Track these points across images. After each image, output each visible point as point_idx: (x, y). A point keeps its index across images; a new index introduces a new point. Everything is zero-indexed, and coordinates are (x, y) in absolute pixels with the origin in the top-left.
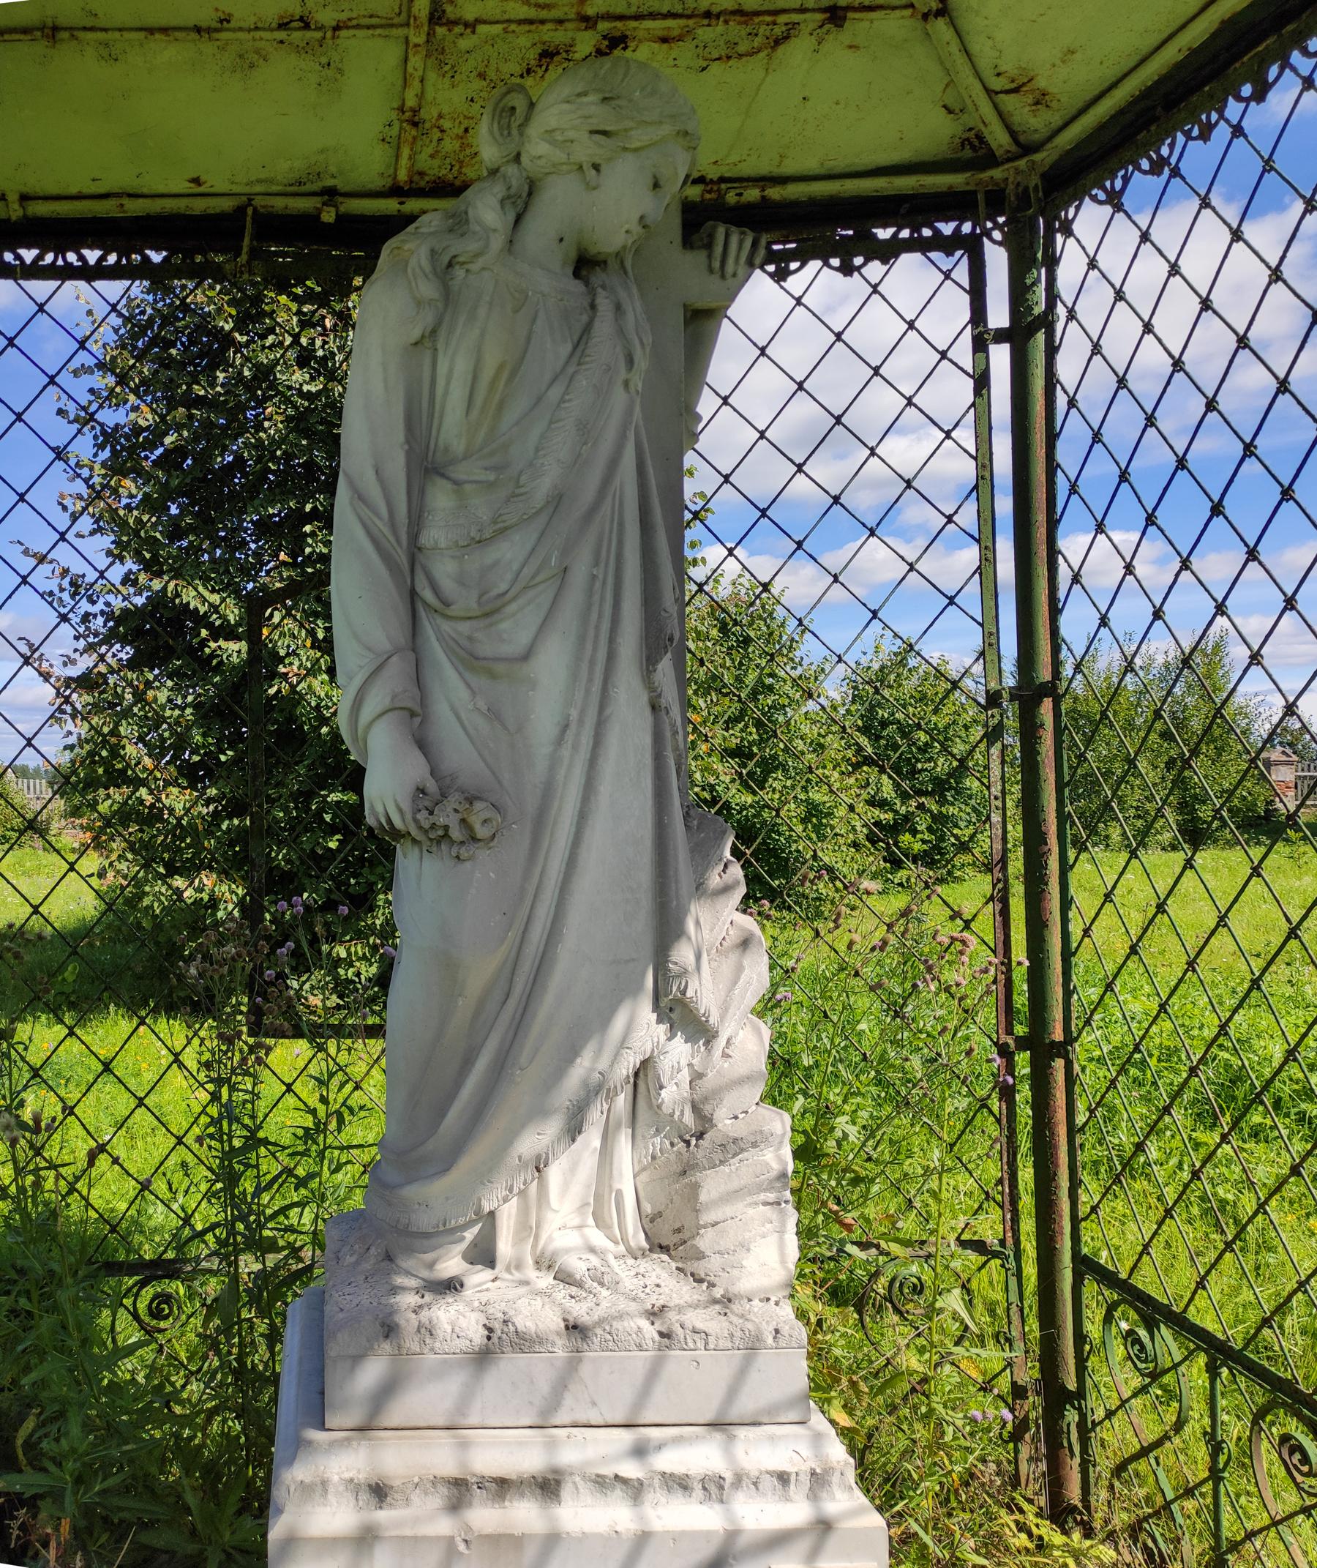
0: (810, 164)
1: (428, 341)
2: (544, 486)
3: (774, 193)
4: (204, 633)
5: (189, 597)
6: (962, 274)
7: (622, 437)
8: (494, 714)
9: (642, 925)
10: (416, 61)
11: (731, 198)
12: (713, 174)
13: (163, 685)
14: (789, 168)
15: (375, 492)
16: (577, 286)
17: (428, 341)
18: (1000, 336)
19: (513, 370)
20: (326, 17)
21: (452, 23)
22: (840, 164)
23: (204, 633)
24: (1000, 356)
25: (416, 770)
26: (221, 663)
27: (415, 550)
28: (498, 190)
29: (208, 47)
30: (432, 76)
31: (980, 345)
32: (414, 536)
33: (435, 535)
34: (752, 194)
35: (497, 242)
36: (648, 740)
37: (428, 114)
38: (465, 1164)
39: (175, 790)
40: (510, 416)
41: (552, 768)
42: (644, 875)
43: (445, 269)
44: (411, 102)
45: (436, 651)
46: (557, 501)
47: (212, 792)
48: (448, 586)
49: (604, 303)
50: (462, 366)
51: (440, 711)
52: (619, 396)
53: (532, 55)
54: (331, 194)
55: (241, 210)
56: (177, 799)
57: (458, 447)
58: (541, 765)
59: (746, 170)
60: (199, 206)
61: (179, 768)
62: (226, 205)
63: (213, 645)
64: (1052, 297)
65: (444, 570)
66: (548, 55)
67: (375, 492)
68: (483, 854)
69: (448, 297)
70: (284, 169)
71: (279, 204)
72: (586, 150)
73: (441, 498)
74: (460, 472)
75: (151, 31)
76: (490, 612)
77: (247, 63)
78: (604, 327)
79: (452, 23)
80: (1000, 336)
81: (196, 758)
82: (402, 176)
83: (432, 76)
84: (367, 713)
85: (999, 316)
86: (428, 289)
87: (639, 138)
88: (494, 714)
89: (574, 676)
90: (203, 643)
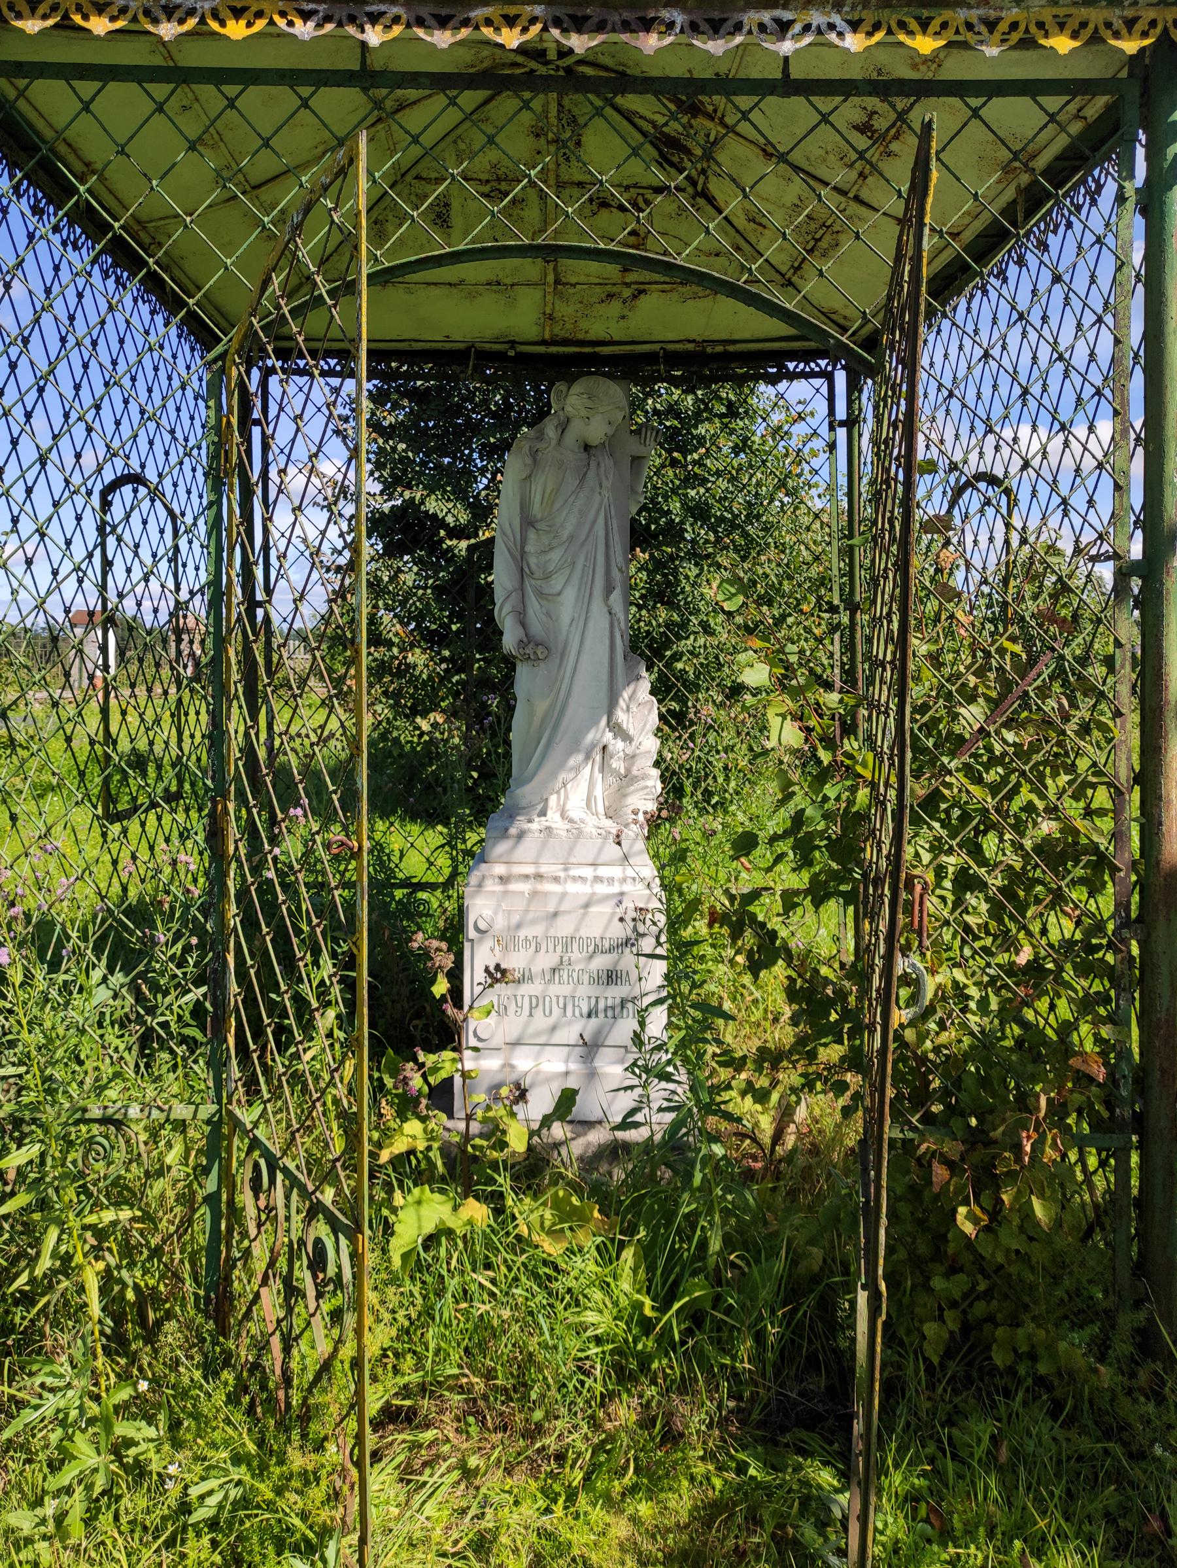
0: (747, 335)
1: (529, 478)
2: (566, 534)
3: (731, 348)
4: (442, 533)
5: (433, 505)
6: (824, 390)
7: (598, 513)
8: (548, 614)
9: (603, 695)
10: (549, 298)
11: (709, 350)
12: (699, 339)
13: (410, 569)
14: (736, 337)
15: (509, 532)
16: (585, 455)
17: (529, 478)
18: (842, 424)
19: (557, 490)
20: (509, 281)
21: (565, 284)
22: (762, 336)
23: (442, 533)
24: (842, 433)
25: (520, 633)
26: (454, 555)
27: (523, 553)
28: (555, 422)
29: (454, 290)
30: (557, 302)
31: (832, 428)
32: (523, 548)
33: (529, 548)
34: (719, 349)
35: (554, 443)
36: (607, 626)
37: (557, 315)
38: (537, 779)
39: (418, 651)
40: (557, 506)
41: (569, 632)
42: (605, 676)
43: (534, 454)
44: (548, 311)
45: (529, 590)
46: (571, 538)
47: (446, 653)
48: (534, 567)
49: (593, 464)
50: (540, 488)
51: (530, 612)
52: (597, 498)
53: (603, 296)
54: (513, 343)
55: (468, 349)
56: (417, 658)
57: (539, 516)
58: (564, 633)
59: (715, 337)
60: (448, 346)
61: (421, 634)
62: (462, 346)
63: (449, 543)
64: (860, 410)
65: (533, 561)
66: (610, 296)
67: (509, 532)
68: (542, 664)
69: (535, 461)
70: (489, 334)
71: (488, 346)
72: (584, 413)
73: (532, 535)
74: (539, 526)
75: (429, 284)
76: (547, 577)
77: (472, 296)
78: (591, 474)
79: (565, 284)
80: (842, 424)
81: (434, 627)
82: (547, 337)
83: (557, 302)
84: (504, 613)
85: (841, 413)
86: (529, 461)
87: (602, 409)
88: (548, 614)
89: (577, 601)
90: (442, 541)
